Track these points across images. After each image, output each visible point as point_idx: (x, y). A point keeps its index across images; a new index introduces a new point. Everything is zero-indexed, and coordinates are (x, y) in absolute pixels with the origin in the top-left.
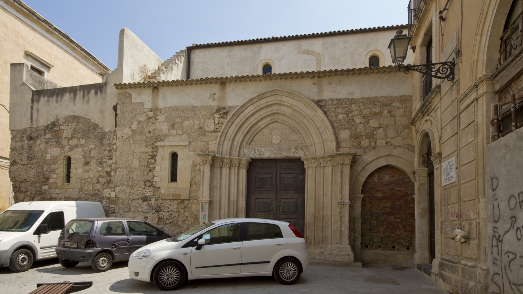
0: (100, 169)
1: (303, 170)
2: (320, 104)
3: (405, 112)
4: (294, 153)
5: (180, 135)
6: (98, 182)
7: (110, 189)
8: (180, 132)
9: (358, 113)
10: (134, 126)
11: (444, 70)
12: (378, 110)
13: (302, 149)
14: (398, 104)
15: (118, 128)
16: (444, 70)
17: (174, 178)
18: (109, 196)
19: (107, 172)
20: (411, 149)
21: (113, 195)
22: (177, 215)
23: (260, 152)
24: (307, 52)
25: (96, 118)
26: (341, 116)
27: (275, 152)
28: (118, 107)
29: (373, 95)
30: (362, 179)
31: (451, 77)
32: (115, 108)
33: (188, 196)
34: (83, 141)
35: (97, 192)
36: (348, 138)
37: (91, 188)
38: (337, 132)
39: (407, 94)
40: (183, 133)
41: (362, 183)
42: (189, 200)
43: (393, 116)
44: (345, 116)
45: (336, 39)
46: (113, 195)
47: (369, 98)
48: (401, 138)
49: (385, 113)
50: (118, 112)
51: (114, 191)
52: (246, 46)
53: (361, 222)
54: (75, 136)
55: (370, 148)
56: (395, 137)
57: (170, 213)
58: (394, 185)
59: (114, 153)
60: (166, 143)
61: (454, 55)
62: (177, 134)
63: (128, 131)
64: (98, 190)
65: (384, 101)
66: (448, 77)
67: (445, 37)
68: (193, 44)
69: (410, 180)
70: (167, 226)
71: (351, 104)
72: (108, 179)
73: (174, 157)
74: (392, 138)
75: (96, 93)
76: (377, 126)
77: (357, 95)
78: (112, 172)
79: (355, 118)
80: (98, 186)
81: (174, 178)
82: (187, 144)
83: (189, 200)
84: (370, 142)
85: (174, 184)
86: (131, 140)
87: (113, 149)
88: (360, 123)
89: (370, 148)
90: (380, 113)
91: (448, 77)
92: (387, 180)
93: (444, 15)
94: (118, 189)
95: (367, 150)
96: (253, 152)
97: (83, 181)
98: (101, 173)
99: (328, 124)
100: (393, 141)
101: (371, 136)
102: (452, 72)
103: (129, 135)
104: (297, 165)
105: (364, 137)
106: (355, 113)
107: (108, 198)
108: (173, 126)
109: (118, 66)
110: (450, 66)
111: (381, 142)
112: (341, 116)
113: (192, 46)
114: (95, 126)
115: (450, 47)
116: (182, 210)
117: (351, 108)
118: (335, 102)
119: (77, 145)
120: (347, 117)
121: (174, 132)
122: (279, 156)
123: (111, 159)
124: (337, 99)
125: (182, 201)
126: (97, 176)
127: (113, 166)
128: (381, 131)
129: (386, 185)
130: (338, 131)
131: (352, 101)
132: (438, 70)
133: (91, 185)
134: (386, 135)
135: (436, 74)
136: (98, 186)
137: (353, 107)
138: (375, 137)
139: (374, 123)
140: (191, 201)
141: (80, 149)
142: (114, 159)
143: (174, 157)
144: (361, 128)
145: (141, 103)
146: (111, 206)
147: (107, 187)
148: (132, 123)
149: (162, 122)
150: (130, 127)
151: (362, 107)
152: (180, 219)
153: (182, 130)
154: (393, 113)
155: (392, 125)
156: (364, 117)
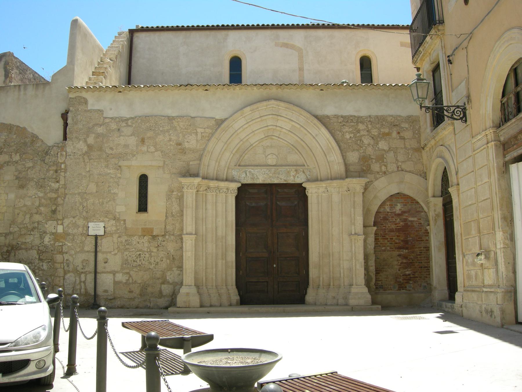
0: (41, 195)
1: (305, 198)
2: (323, 120)
3: (414, 134)
4: (294, 177)
5: (152, 152)
6: (38, 213)
7: (55, 222)
8: (152, 149)
9: (366, 133)
10: (91, 140)
11: (458, 112)
12: (387, 131)
13: (304, 172)
14: (407, 126)
15: (68, 142)
16: (458, 112)
17: (143, 207)
18: (54, 231)
19: (50, 199)
20: (423, 175)
21: (60, 229)
22: (147, 255)
23: (253, 174)
24: (286, 45)
25: (35, 127)
26: (348, 136)
27: (271, 175)
28: (69, 115)
29: (380, 114)
30: (375, 208)
31: (464, 119)
32: (64, 116)
33: (163, 230)
34: (16, 157)
35: (36, 225)
36: (357, 161)
37: (27, 220)
38: (344, 154)
39: (415, 115)
40: (157, 150)
41: (374, 213)
42: (163, 236)
43: (403, 138)
44: (352, 135)
45: (320, 33)
46: (60, 229)
47: (377, 117)
48: (412, 162)
49: (394, 134)
50: (69, 121)
51: (62, 224)
52: (207, 32)
53: (374, 259)
54: (5, 150)
55: (380, 173)
56: (406, 161)
57: (138, 253)
58: (407, 215)
59: (62, 174)
60: (134, 163)
61: (465, 100)
62: (148, 151)
63: (81, 146)
64: (38, 223)
65: (392, 121)
66: (461, 119)
67: (453, 76)
68: (137, 26)
69: (423, 209)
70: (135, 269)
71: (357, 122)
72: (54, 208)
73: (143, 180)
74: (403, 162)
75: (318, 177)
76: (386, 148)
77: (364, 113)
78: (59, 199)
79: (363, 139)
80: (37, 218)
81: (143, 207)
82: (161, 164)
83: (163, 236)
84: (381, 167)
85: (143, 216)
86: (86, 157)
87: (61, 169)
88: (369, 145)
89: (380, 173)
90: (388, 134)
91: (461, 119)
92: (400, 210)
93: (451, 58)
94: (66, 222)
95: (378, 176)
96: (244, 175)
97: (17, 211)
98: (43, 200)
99: (334, 144)
100: (404, 166)
101: (381, 159)
102: (465, 115)
103: (84, 152)
104: (299, 193)
105: (374, 161)
106: (362, 133)
107: (53, 234)
108: (143, 141)
109: (68, 63)
110: (462, 109)
111: (392, 167)
112: (348, 136)
113: (135, 28)
114: (35, 138)
115: (462, 90)
116: (155, 250)
117: (359, 128)
118: (341, 120)
119: (9, 162)
120: (355, 136)
121: (145, 148)
122: (276, 181)
123: (58, 182)
124: (342, 117)
125: (154, 237)
126: (37, 203)
127: (61, 191)
128: (391, 154)
129: (399, 215)
130: (345, 153)
131: (359, 120)
132: (453, 112)
133: (28, 216)
134: (397, 160)
135: (452, 115)
136: (37, 218)
137: (361, 127)
138: (385, 160)
139: (383, 145)
140: (167, 237)
141: (12, 168)
142: (62, 182)
143: (143, 180)
144: (370, 151)
145: (99, 110)
146: (57, 244)
147: (52, 219)
148: (88, 136)
149: (129, 136)
150: (85, 141)
151: (370, 126)
152: (152, 261)
153: (155, 146)
154: (402, 134)
155: (402, 148)
156: (372, 138)
